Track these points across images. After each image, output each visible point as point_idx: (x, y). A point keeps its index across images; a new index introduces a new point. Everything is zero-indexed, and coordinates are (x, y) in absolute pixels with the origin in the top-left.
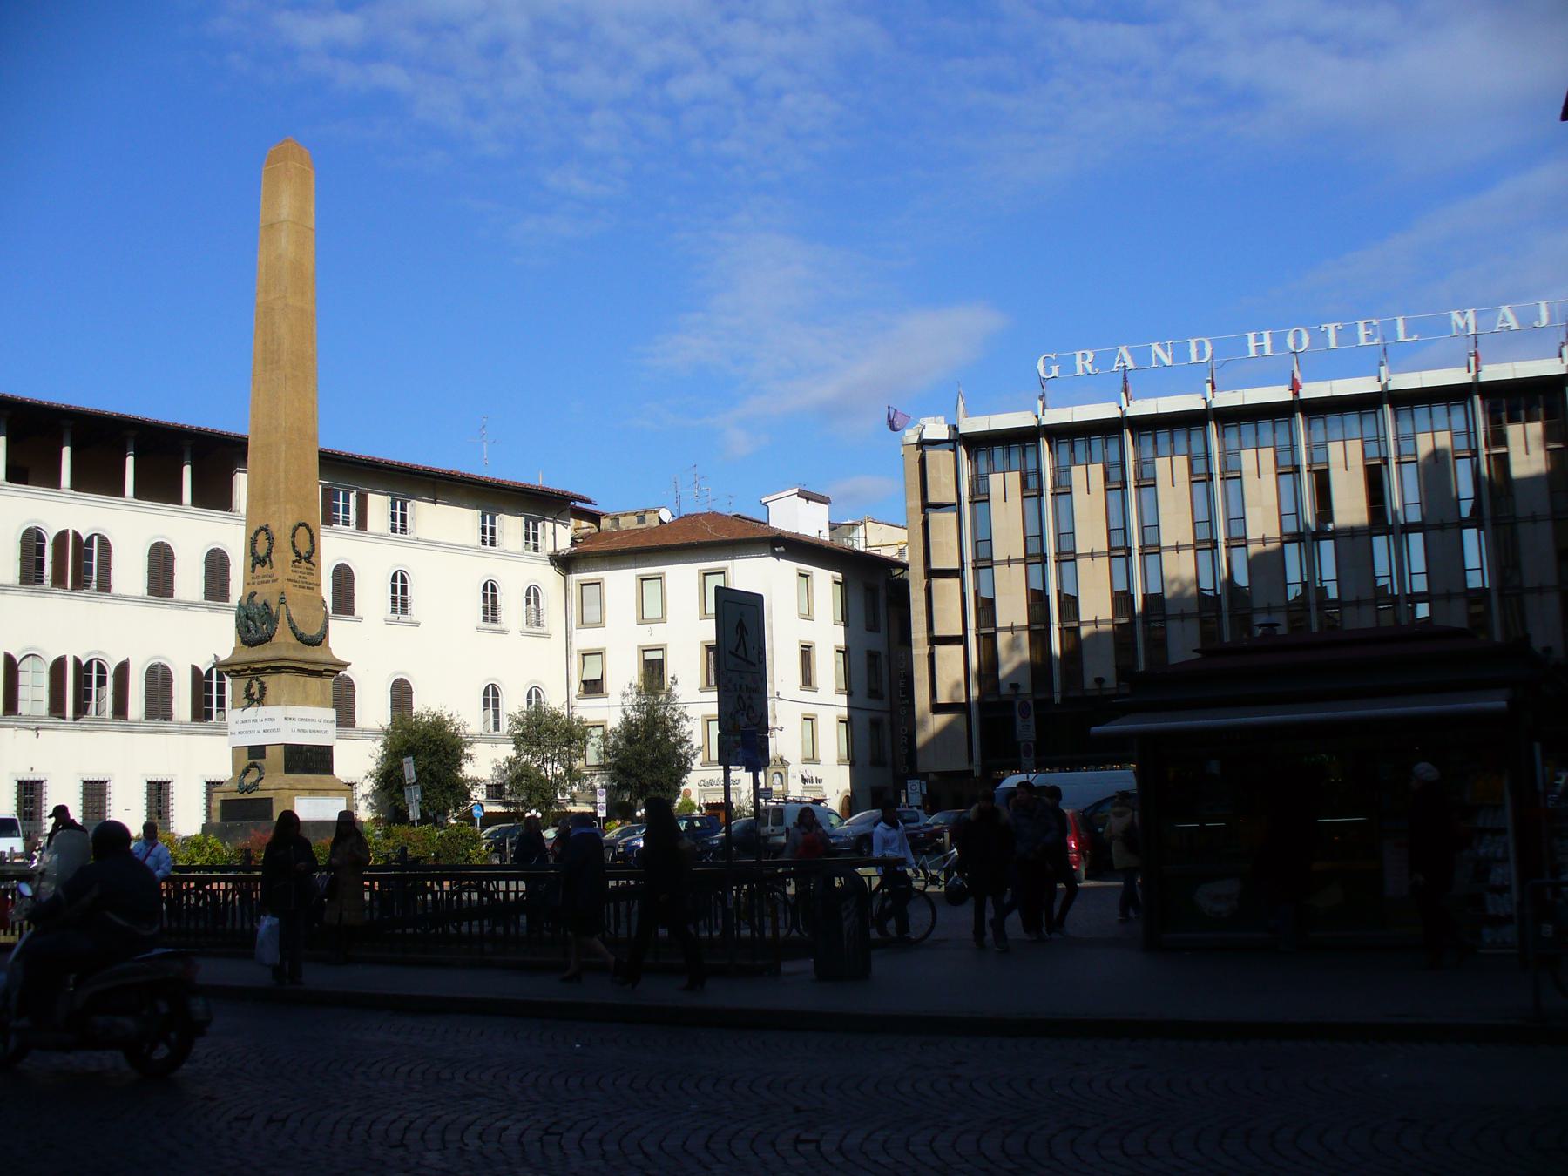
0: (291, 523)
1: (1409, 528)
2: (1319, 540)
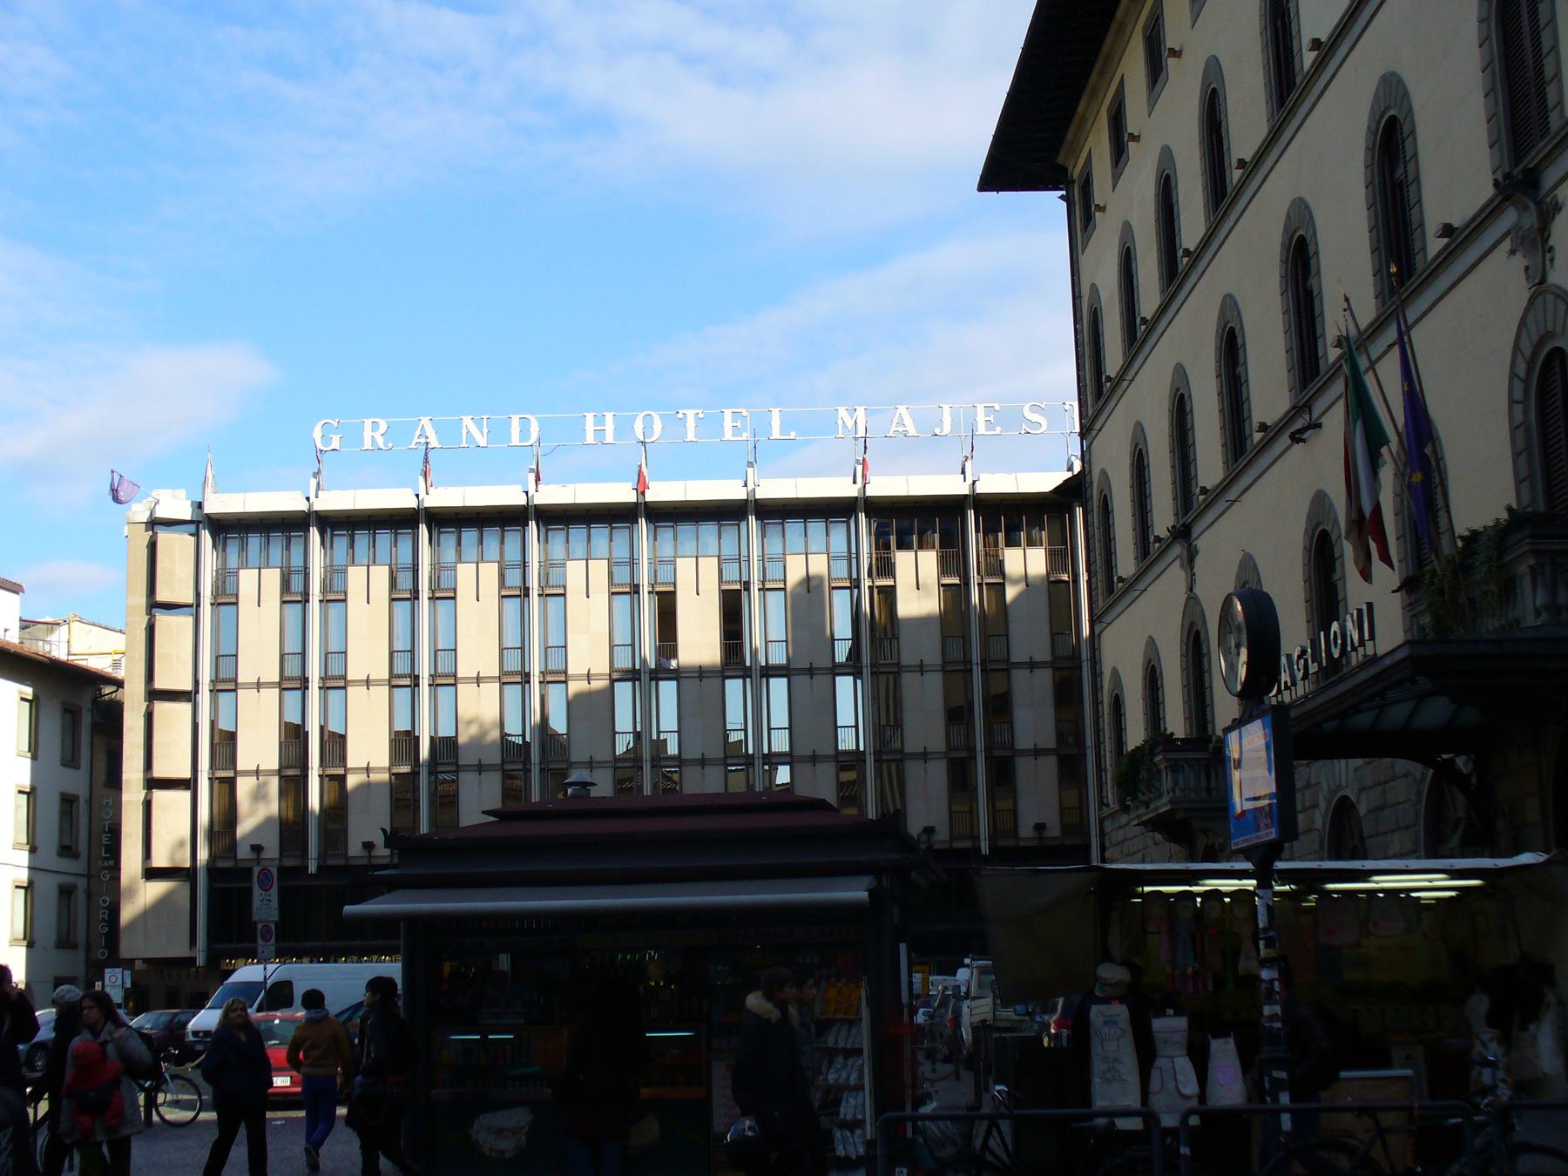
1: (769, 672)
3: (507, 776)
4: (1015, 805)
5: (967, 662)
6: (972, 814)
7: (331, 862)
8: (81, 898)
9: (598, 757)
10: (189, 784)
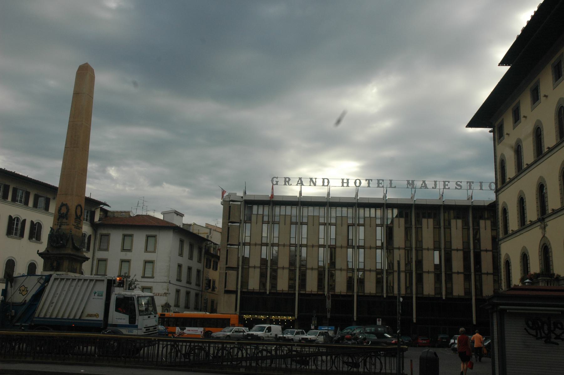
0: (76, 204)
1: (359, 247)
2: (273, 246)
3: (290, 270)
4: (452, 286)
5: (411, 248)
6: (441, 288)
7: (272, 291)
8: (200, 296)
9: (372, 269)
10: (236, 269)
